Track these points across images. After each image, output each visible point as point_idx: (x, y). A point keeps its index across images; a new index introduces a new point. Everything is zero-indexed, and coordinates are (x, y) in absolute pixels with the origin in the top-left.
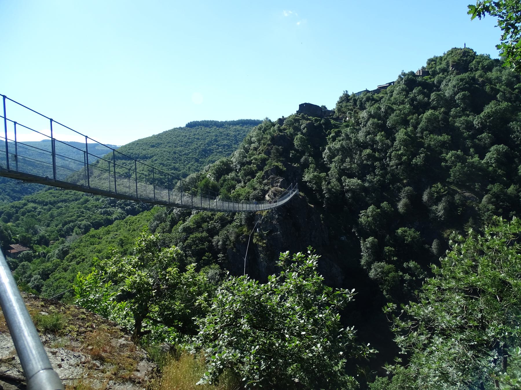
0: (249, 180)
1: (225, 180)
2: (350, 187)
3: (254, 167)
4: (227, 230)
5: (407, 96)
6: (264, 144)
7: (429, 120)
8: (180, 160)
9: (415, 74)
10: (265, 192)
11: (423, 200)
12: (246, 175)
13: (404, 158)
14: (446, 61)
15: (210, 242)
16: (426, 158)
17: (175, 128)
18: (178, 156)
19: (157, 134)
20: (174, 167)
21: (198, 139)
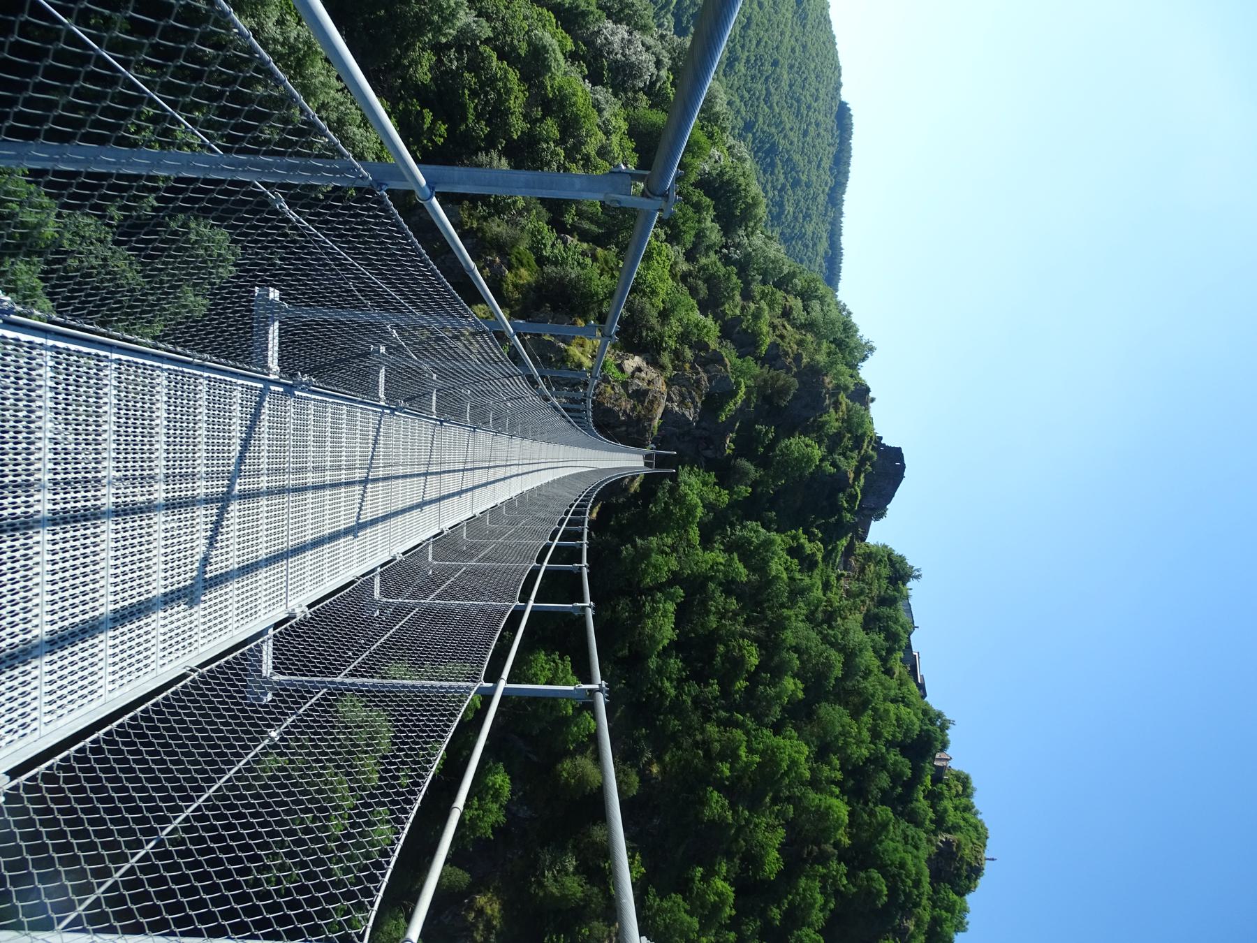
0: (693, 292)
1: (698, 207)
2: (648, 617)
3: (732, 308)
4: (527, 209)
5: (890, 744)
6: (800, 343)
7: (824, 814)
8: (753, 77)
10: (650, 351)
11: (594, 824)
12: (711, 280)
13: (725, 769)
14: (962, 823)
15: (490, 143)
16: (718, 825)
17: (840, 70)
18: (766, 74)
19: (832, 17)
20: (737, 59)
21: (805, 133)
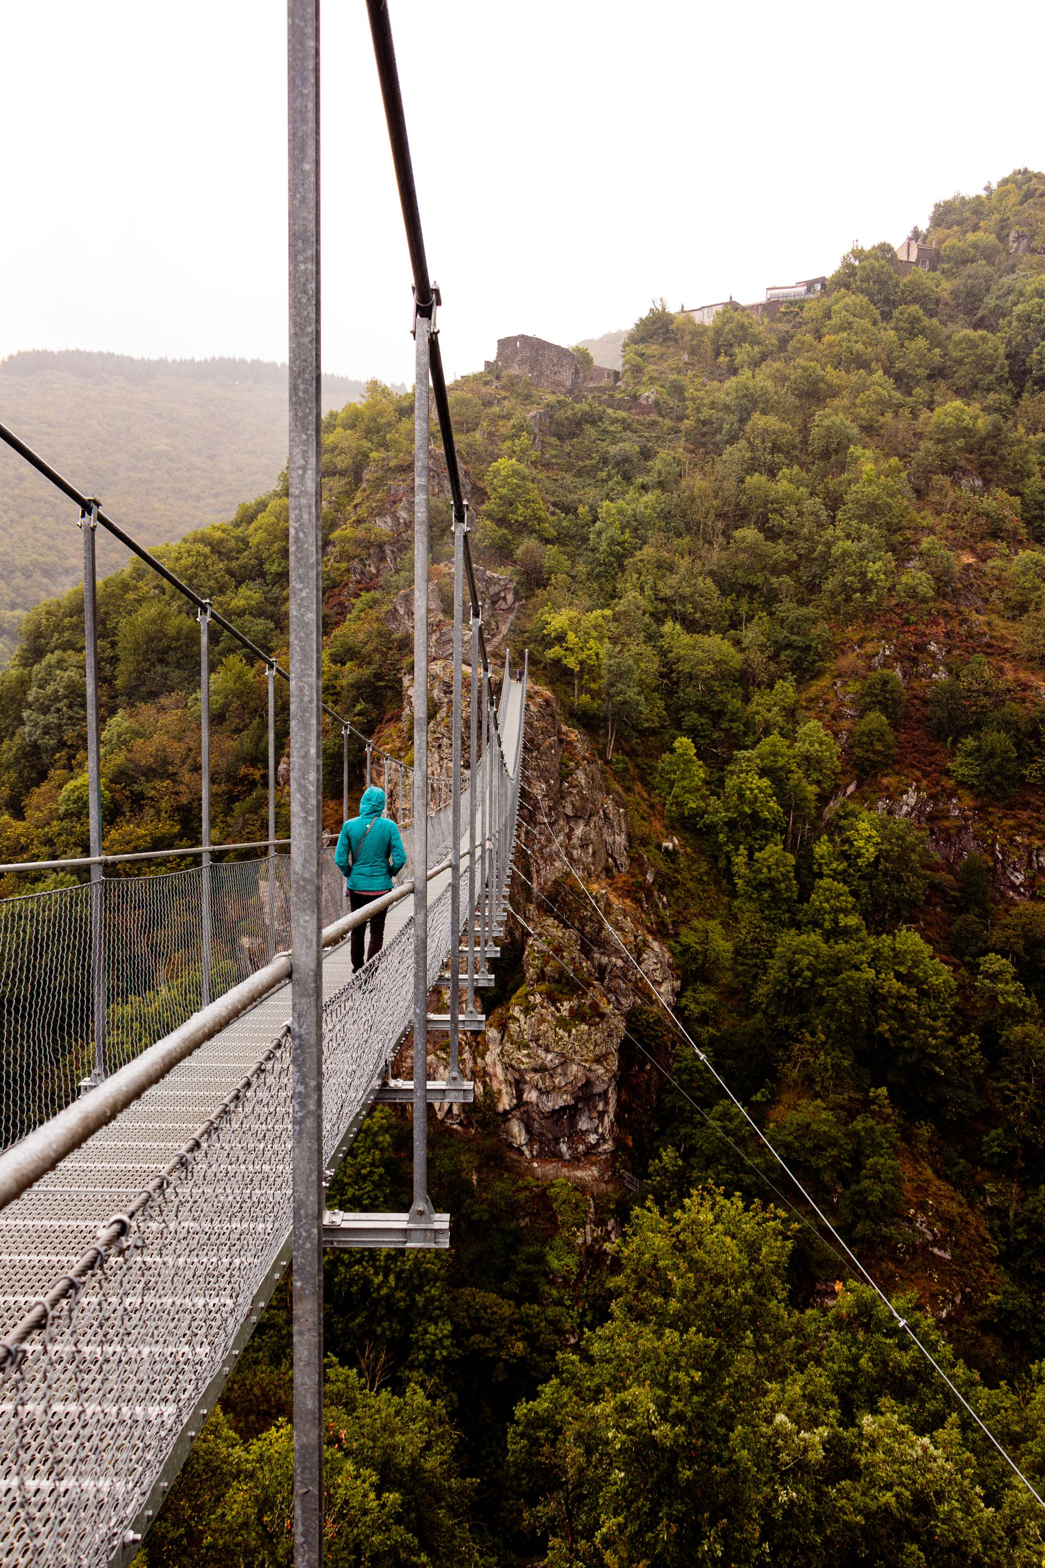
9: (894, 255)
